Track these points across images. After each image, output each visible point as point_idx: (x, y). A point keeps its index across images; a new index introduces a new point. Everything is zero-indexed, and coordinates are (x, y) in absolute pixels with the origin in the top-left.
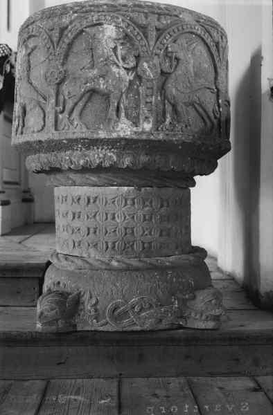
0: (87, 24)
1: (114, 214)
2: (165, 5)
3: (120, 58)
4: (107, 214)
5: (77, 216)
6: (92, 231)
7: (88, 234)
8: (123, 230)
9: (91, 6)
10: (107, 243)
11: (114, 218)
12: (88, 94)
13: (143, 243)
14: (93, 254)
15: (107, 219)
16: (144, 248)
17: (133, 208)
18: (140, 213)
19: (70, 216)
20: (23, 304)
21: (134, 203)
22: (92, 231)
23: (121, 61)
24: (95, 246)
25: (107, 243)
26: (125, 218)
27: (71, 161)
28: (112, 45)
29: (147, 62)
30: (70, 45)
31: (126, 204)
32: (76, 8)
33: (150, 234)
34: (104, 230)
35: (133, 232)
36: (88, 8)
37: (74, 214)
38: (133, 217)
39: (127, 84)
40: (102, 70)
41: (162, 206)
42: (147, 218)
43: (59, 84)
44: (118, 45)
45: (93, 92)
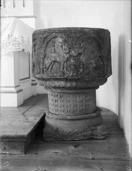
0: (52, 37)
1: (70, 101)
2: (81, 28)
3: (64, 49)
4: (67, 101)
5: (56, 101)
6: (62, 106)
7: (61, 107)
8: (73, 106)
9: (53, 31)
10: (67, 110)
11: (69, 102)
12: (53, 63)
13: (80, 110)
14: (63, 113)
15: (67, 102)
16: (80, 111)
17: (76, 98)
18: (78, 100)
19: (54, 101)
20: (79, 141)
21: (76, 97)
22: (62, 106)
23: (64, 50)
24: (64, 111)
25: (67, 110)
26: (73, 102)
27: (49, 85)
28: (61, 45)
29: (74, 50)
30: (47, 43)
31: (73, 97)
32: (49, 32)
33: (82, 106)
34: (66, 106)
35: (76, 106)
36: (53, 32)
37: (56, 100)
38: (76, 102)
39: (66, 59)
40: (40, 76)
41: (86, 97)
42: (81, 101)
43: (44, 58)
44: (63, 45)
45: (55, 61)
